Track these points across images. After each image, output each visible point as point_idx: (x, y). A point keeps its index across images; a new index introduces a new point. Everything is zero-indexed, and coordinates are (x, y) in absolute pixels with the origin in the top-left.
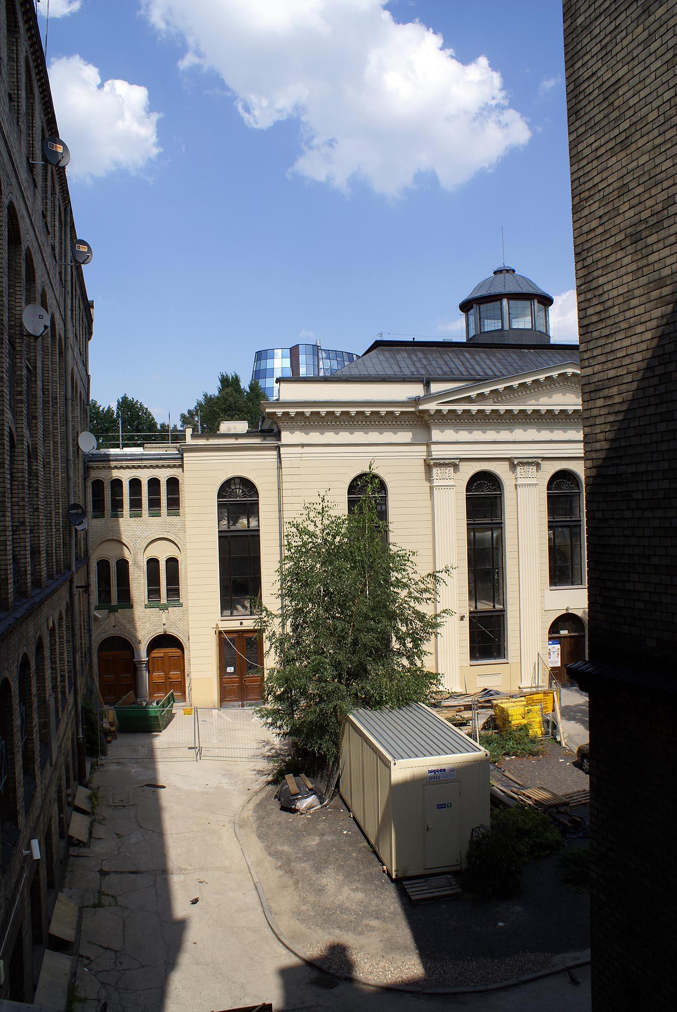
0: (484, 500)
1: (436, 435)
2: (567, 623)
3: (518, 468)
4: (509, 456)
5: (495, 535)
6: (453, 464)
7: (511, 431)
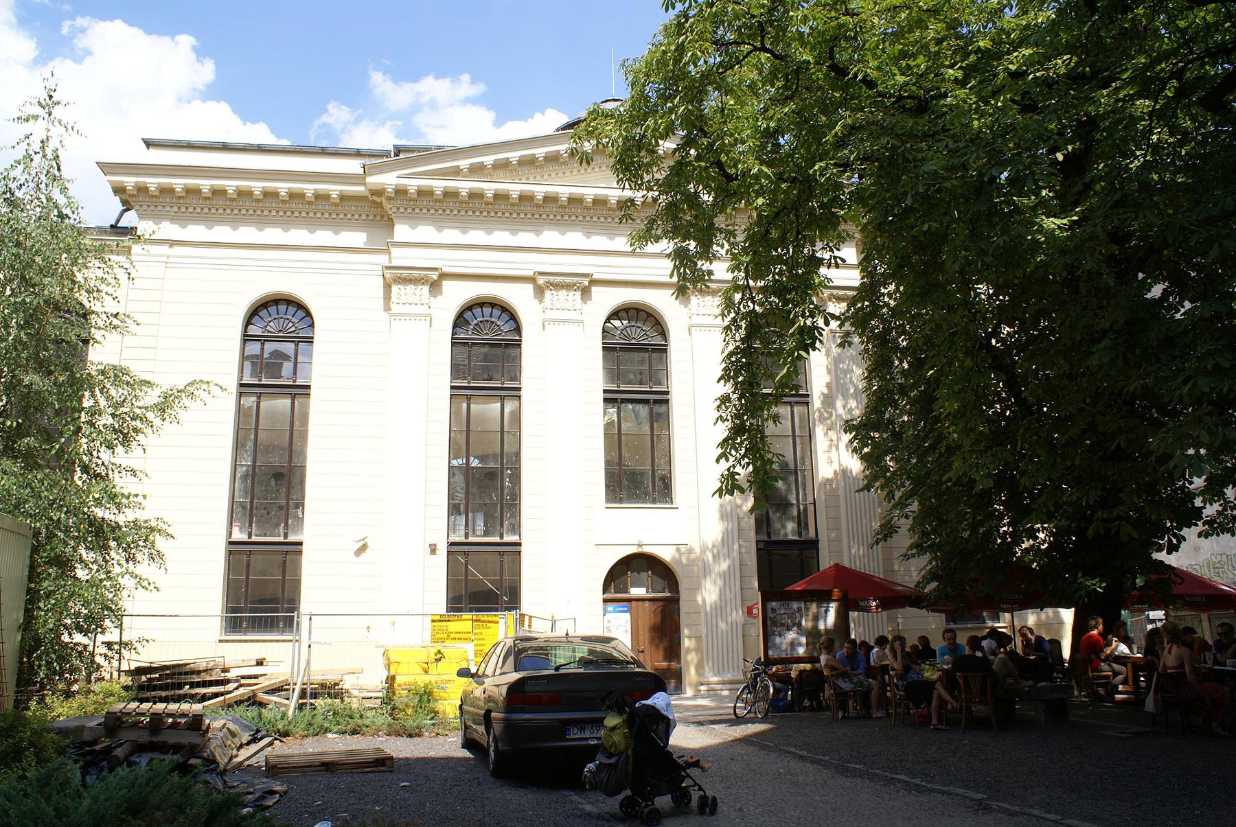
0: (486, 348)
1: (402, 231)
2: (644, 575)
3: (548, 293)
4: (530, 273)
5: (507, 411)
6: (435, 281)
7: (538, 233)
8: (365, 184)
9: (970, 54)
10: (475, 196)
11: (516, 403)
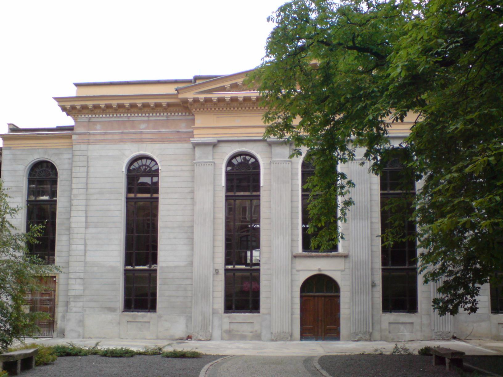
8: (177, 98)
9: (447, 22)
10: (234, 100)
11: (157, 178)
